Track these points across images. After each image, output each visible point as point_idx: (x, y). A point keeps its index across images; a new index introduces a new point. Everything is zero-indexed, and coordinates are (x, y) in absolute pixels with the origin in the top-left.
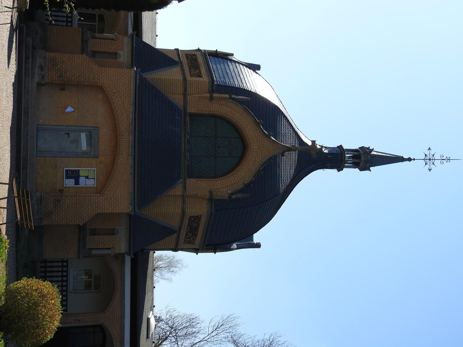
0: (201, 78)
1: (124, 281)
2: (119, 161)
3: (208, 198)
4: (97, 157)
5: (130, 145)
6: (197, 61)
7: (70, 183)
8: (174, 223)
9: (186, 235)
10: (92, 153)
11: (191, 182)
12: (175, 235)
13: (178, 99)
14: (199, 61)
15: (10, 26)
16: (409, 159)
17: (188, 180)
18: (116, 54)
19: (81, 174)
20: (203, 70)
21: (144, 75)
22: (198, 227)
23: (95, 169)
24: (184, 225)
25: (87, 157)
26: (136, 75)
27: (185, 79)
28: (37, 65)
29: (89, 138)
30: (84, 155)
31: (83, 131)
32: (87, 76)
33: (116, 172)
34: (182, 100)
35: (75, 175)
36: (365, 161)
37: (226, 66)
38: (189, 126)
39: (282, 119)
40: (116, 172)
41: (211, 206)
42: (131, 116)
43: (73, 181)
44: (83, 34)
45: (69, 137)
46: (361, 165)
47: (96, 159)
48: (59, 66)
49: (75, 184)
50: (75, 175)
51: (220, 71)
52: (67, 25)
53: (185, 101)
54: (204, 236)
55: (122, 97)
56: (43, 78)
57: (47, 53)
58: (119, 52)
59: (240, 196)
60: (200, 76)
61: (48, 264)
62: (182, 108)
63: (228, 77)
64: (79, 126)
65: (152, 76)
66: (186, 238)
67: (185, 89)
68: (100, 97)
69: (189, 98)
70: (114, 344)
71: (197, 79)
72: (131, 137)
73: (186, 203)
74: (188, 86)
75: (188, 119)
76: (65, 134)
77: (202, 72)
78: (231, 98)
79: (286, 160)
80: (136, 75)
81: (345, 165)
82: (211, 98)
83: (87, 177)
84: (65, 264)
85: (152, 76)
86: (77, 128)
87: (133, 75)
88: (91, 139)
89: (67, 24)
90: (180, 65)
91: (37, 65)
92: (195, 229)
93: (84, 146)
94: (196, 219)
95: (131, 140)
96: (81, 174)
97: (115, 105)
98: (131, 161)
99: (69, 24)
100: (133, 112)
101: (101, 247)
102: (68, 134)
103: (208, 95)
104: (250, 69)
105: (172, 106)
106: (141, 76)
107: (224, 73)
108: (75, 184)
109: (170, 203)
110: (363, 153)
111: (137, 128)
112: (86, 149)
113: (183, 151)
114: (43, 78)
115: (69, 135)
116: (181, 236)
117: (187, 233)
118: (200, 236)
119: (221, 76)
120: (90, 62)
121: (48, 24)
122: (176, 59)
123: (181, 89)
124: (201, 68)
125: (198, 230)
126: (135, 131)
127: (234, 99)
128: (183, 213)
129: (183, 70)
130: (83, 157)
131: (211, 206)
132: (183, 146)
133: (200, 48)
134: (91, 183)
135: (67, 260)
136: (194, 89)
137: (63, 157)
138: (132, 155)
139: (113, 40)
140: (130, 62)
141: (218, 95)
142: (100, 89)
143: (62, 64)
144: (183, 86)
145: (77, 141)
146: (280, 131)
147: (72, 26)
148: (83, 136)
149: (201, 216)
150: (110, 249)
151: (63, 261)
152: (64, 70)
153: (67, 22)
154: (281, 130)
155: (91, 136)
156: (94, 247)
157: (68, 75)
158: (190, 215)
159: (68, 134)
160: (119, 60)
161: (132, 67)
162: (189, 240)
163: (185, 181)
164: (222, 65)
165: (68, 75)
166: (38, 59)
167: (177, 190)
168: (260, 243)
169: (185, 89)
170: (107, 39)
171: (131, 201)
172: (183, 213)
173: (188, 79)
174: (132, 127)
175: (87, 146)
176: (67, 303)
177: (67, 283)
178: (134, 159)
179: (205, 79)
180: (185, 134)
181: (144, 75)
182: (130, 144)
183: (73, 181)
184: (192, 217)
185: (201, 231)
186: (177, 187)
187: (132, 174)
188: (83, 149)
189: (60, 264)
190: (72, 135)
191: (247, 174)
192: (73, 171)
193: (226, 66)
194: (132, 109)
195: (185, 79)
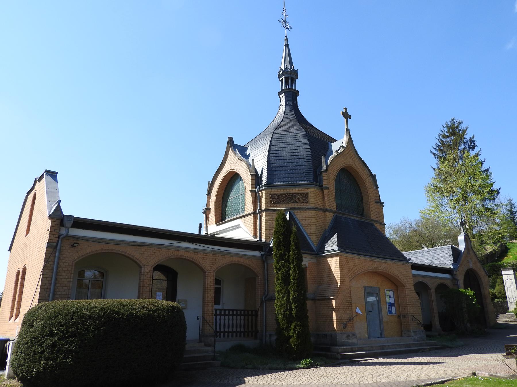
0: (310, 194)
28: (347, 340)
33: (166, 256)
40: (166, 256)
45: (371, 312)
46: (294, 76)
63: (278, 168)
77: (299, 192)
81: (293, 88)
98: (389, 261)
102: (369, 312)
110: (290, 74)
115: (370, 312)
135: (215, 309)
144: (319, 211)
157: (348, 312)
159: (369, 312)
166: (343, 340)
168: (229, 137)
174: (373, 259)
175: (373, 296)
177: (231, 310)
187: (386, 260)
188: (375, 300)
189: (218, 317)
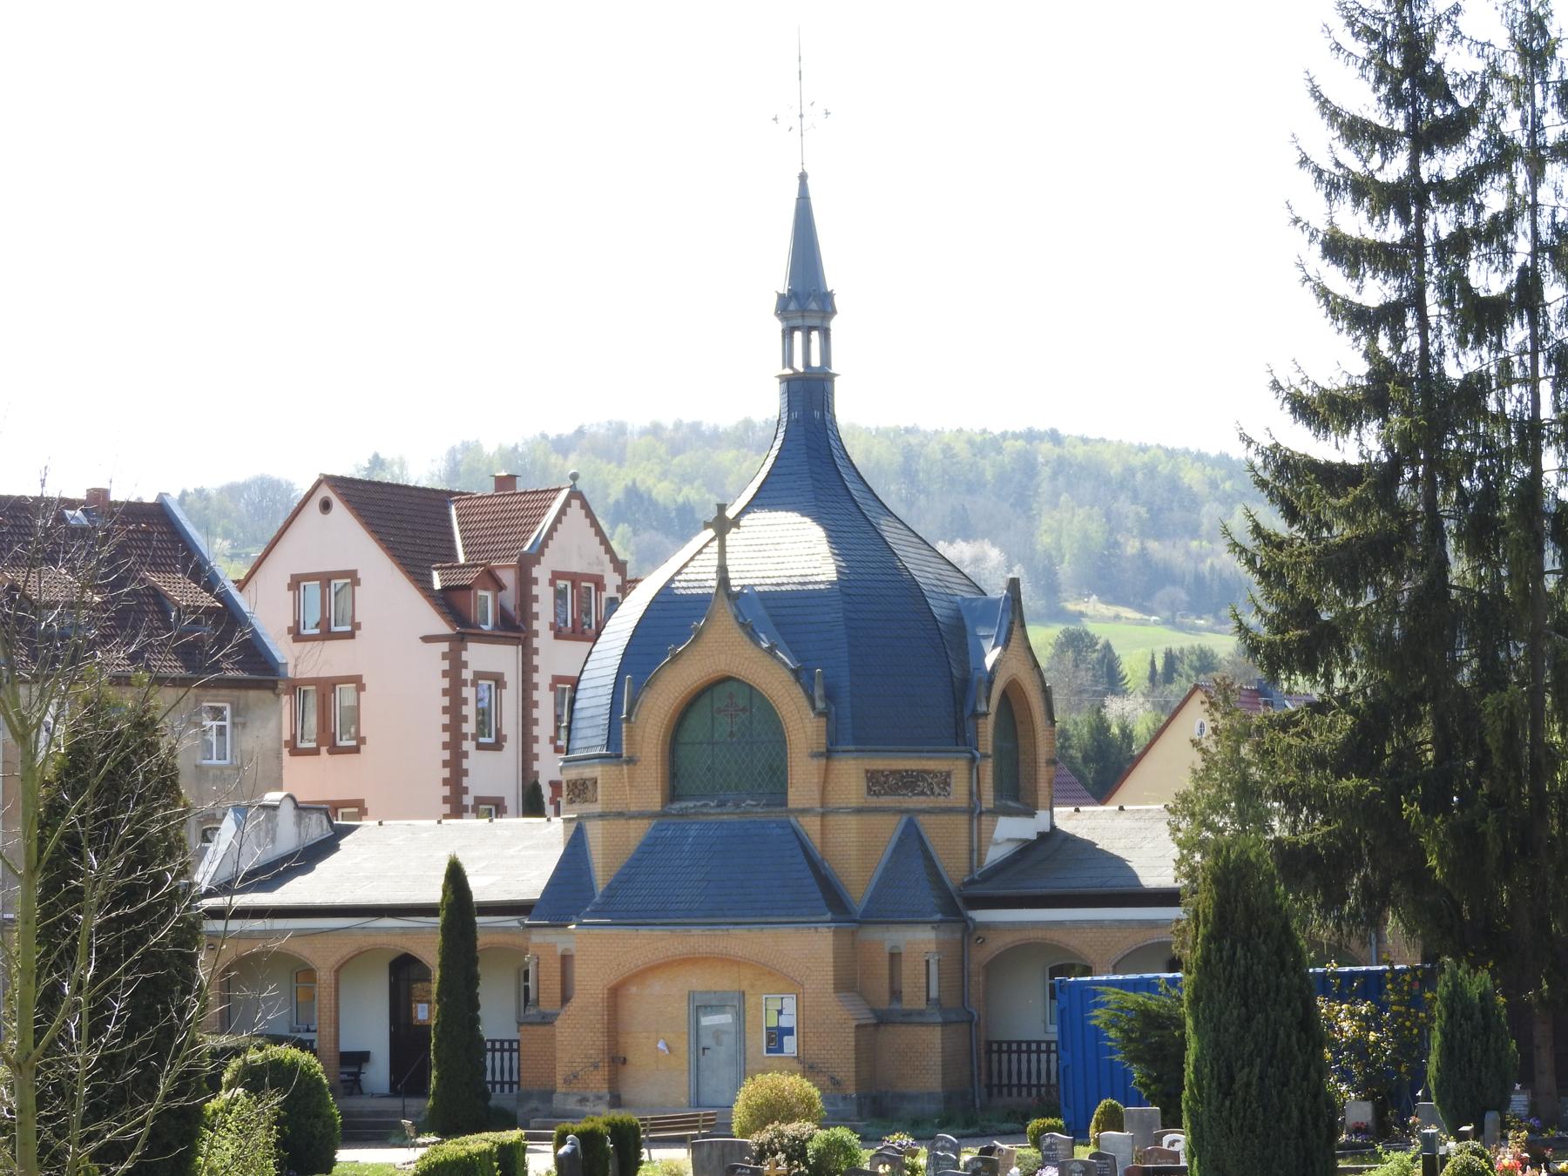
1: (1013, 923)
2: (740, 954)
3: (824, 761)
4: (743, 993)
5: (710, 933)
7: (790, 1043)
8: (888, 828)
9: (923, 793)
12: (924, 822)
13: (637, 831)
16: (803, 178)
17: (791, 805)
19: (773, 1023)
22: (893, 772)
23: (764, 997)
24: (893, 805)
25: (744, 1012)
27: (602, 816)
28: (580, 1108)
29: (709, 1009)
30: (740, 1017)
32: (592, 1017)
34: (638, 821)
36: (803, 317)
38: (691, 804)
41: (843, 751)
42: (658, 932)
44: (531, 1024)
47: (746, 996)
48: (578, 1069)
49: (792, 1034)
52: (518, 1050)
54: (925, 754)
55: (625, 950)
56: (600, 1098)
57: (558, 1090)
58: (559, 952)
59: (818, 692)
61: (995, 1081)
62: (654, 822)
64: (689, 1029)
65: (601, 877)
66: (933, 793)
67: (620, 815)
68: (634, 989)
70: (1156, 940)
72: (696, 931)
73: (838, 805)
74: (614, 810)
75: (677, 806)
76: (704, 1054)
78: (628, 720)
82: (631, 761)
83: (780, 1012)
84: (995, 1047)
85: (601, 877)
86: (692, 1032)
87: (584, 930)
88: (711, 1006)
89: (515, 1050)
91: (580, 1108)
92: (903, 777)
93: (725, 1019)
94: (876, 782)
96: (775, 1025)
97: (640, 963)
99: (515, 1046)
100: (651, 930)
101: (924, 980)
102: (704, 1049)
105: (648, 848)
108: (792, 1034)
109: (839, 840)
112: (729, 1016)
113: (735, 818)
114: (600, 1098)
116: (924, 806)
117: (915, 795)
118: (924, 762)
120: (569, 1013)
121: (519, 1088)
122: (573, 825)
125: (906, 771)
127: (629, 713)
128: (859, 811)
130: (744, 1021)
131: (843, 751)
132: (725, 817)
134: (790, 1004)
136: (617, 797)
137: (745, 1058)
138: (727, 930)
139: (538, 963)
142: (615, 994)
143: (575, 1065)
145: (717, 1032)
147: (518, 1041)
148: (707, 1021)
149: (867, 771)
150: (928, 961)
151: (989, 1051)
152: (585, 1060)
153: (511, 1050)
155: (706, 1007)
156: (925, 994)
157: (592, 1052)
158: (865, 796)
162: (938, 785)
163: (792, 811)
165: (592, 1052)
166: (569, 1107)
167: (811, 827)
169: (620, 815)
170: (538, 976)
171: (809, 928)
172: (859, 811)
173: (600, 810)
175: (724, 1013)
176: (1034, 1042)
180: (703, 814)
182: (707, 933)
184: (869, 788)
185: (911, 762)
186: (806, 828)
187: (762, 929)
189: (995, 1057)
191: (776, 675)
192: (770, 1040)
194: (644, 931)
195: (602, 816)
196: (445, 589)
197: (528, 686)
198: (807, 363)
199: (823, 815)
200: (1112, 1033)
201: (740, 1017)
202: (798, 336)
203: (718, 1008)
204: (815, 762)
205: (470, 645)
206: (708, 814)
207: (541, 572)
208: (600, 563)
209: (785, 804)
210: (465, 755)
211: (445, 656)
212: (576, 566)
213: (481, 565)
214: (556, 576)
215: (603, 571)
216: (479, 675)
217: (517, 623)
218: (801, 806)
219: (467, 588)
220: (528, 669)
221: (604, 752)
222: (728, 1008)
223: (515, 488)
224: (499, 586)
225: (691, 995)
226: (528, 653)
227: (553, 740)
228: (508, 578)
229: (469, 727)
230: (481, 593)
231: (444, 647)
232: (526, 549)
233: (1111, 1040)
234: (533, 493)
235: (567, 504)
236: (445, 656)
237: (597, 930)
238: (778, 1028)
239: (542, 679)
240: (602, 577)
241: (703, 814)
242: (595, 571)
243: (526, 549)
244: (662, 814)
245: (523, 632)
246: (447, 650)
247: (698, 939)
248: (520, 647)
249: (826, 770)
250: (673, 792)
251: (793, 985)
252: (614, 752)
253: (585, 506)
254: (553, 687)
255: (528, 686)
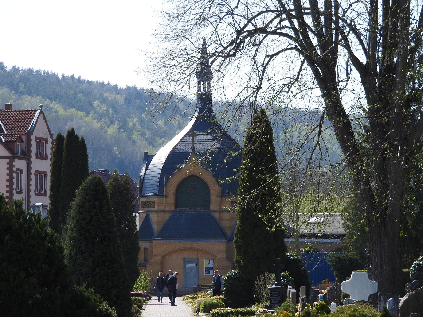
4: (199, 258)
6: (146, 202)
7: (211, 272)
10: (196, 261)
11: (212, 208)
13: (167, 216)
14: (145, 201)
15: (137, 278)
17: (211, 209)
18: (145, 249)
20: (151, 199)
21: (155, 235)
26: (156, 239)
27: (157, 211)
30: (197, 265)
31: (186, 266)
34: (168, 213)
35: (208, 270)
37: (148, 184)
38: (182, 209)
39: (177, 149)
42: (177, 242)
43: (210, 271)
50: (208, 270)
51: (151, 189)
53: (168, 211)
60: (154, 202)
67: (162, 211)
68: (168, 257)
69: (166, 209)
71: (156, 204)
72: (188, 242)
75: (178, 209)
78: (166, 186)
79: (202, 144)
80: (156, 239)
82: (166, 197)
83: (209, 263)
87: (155, 241)
90: (148, 213)
93: (193, 265)
95: (188, 242)
96: (207, 267)
103: (164, 199)
104: (150, 163)
105: (171, 219)
106: (156, 237)
107: (151, 186)
111: (183, 239)
113: (195, 212)
119: (153, 189)
123: (162, 214)
124: (149, 200)
126: (184, 240)
127: (166, 184)
129: (151, 211)
132: (193, 212)
133: (129, 86)
134: (212, 262)
140: (149, 241)
141: (164, 192)
145: (191, 269)
146: (184, 150)
148: (188, 266)
154: (184, 149)
155: (188, 262)
160: (148, 248)
161: (152, 241)
163: (211, 211)
164: (147, 186)
167: (217, 215)
169: (162, 211)
175: (193, 263)
178: (199, 240)
179: (155, 199)
180: (186, 211)
181: (155, 235)
183: (210, 271)
190: (187, 271)
193: (148, 184)
194: (173, 242)
195: (157, 211)
196: (6, 142)
197: (29, 174)
198: (205, 90)
199: (220, 212)
200: (330, 263)
201: (197, 265)
202: (202, 83)
203: (192, 262)
204: (219, 198)
205: (16, 160)
206: (188, 211)
207: (33, 137)
208: (47, 135)
209: (210, 209)
210: (13, 195)
211: (8, 163)
212: (41, 135)
213: (18, 134)
214: (37, 138)
215: (48, 137)
216: (17, 169)
217: (26, 153)
218: (214, 210)
219: (15, 141)
220: (29, 168)
221: (157, 194)
222: (194, 263)
223: (11, 109)
224: (22, 141)
225: (184, 259)
226: (29, 163)
227: (35, 191)
228: (24, 138)
229: (14, 186)
230: (18, 143)
231: (8, 160)
232: (29, 129)
233: (329, 265)
234: (26, 111)
235: (39, 115)
236: (8, 163)
237: (160, 241)
238: (208, 267)
239: (33, 171)
240: (47, 139)
241: (186, 211)
242: (45, 137)
243: (29, 129)
244: (175, 211)
245: (28, 156)
246: (8, 161)
247: (188, 244)
248: (27, 161)
249: (221, 200)
250: (176, 207)
251: (213, 256)
252: (161, 193)
253: (44, 116)
254: (35, 174)
255: (29, 174)
